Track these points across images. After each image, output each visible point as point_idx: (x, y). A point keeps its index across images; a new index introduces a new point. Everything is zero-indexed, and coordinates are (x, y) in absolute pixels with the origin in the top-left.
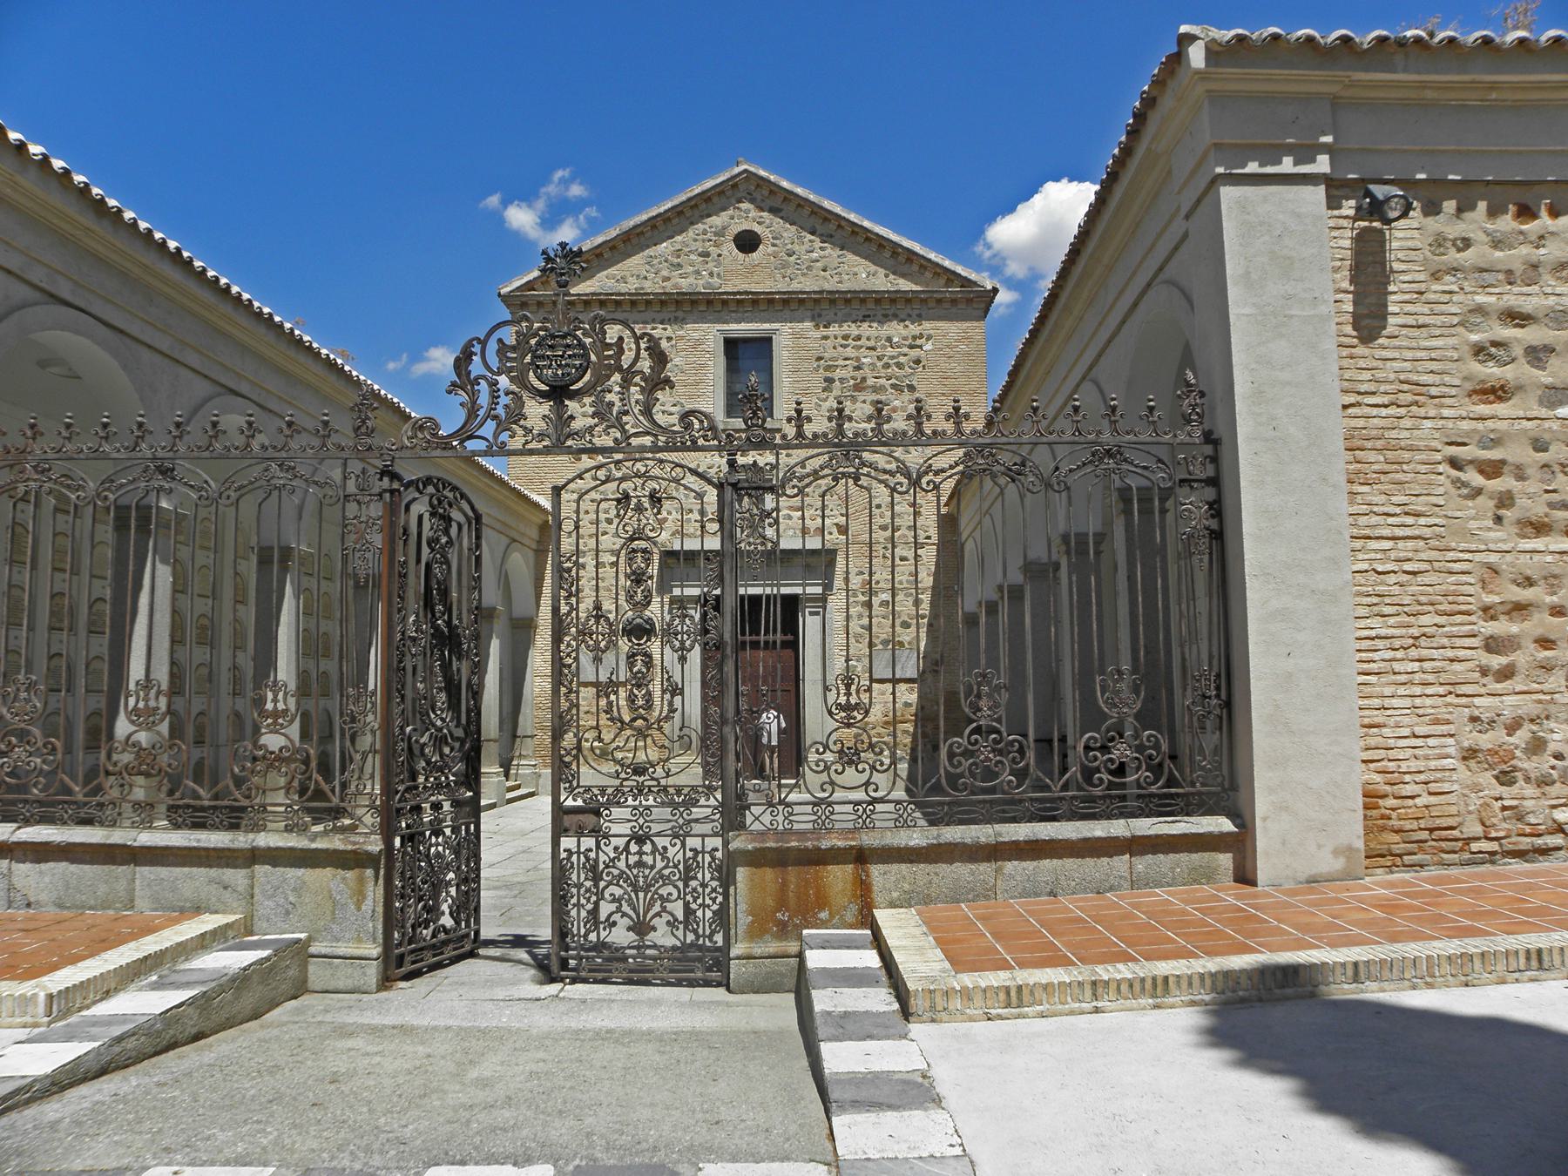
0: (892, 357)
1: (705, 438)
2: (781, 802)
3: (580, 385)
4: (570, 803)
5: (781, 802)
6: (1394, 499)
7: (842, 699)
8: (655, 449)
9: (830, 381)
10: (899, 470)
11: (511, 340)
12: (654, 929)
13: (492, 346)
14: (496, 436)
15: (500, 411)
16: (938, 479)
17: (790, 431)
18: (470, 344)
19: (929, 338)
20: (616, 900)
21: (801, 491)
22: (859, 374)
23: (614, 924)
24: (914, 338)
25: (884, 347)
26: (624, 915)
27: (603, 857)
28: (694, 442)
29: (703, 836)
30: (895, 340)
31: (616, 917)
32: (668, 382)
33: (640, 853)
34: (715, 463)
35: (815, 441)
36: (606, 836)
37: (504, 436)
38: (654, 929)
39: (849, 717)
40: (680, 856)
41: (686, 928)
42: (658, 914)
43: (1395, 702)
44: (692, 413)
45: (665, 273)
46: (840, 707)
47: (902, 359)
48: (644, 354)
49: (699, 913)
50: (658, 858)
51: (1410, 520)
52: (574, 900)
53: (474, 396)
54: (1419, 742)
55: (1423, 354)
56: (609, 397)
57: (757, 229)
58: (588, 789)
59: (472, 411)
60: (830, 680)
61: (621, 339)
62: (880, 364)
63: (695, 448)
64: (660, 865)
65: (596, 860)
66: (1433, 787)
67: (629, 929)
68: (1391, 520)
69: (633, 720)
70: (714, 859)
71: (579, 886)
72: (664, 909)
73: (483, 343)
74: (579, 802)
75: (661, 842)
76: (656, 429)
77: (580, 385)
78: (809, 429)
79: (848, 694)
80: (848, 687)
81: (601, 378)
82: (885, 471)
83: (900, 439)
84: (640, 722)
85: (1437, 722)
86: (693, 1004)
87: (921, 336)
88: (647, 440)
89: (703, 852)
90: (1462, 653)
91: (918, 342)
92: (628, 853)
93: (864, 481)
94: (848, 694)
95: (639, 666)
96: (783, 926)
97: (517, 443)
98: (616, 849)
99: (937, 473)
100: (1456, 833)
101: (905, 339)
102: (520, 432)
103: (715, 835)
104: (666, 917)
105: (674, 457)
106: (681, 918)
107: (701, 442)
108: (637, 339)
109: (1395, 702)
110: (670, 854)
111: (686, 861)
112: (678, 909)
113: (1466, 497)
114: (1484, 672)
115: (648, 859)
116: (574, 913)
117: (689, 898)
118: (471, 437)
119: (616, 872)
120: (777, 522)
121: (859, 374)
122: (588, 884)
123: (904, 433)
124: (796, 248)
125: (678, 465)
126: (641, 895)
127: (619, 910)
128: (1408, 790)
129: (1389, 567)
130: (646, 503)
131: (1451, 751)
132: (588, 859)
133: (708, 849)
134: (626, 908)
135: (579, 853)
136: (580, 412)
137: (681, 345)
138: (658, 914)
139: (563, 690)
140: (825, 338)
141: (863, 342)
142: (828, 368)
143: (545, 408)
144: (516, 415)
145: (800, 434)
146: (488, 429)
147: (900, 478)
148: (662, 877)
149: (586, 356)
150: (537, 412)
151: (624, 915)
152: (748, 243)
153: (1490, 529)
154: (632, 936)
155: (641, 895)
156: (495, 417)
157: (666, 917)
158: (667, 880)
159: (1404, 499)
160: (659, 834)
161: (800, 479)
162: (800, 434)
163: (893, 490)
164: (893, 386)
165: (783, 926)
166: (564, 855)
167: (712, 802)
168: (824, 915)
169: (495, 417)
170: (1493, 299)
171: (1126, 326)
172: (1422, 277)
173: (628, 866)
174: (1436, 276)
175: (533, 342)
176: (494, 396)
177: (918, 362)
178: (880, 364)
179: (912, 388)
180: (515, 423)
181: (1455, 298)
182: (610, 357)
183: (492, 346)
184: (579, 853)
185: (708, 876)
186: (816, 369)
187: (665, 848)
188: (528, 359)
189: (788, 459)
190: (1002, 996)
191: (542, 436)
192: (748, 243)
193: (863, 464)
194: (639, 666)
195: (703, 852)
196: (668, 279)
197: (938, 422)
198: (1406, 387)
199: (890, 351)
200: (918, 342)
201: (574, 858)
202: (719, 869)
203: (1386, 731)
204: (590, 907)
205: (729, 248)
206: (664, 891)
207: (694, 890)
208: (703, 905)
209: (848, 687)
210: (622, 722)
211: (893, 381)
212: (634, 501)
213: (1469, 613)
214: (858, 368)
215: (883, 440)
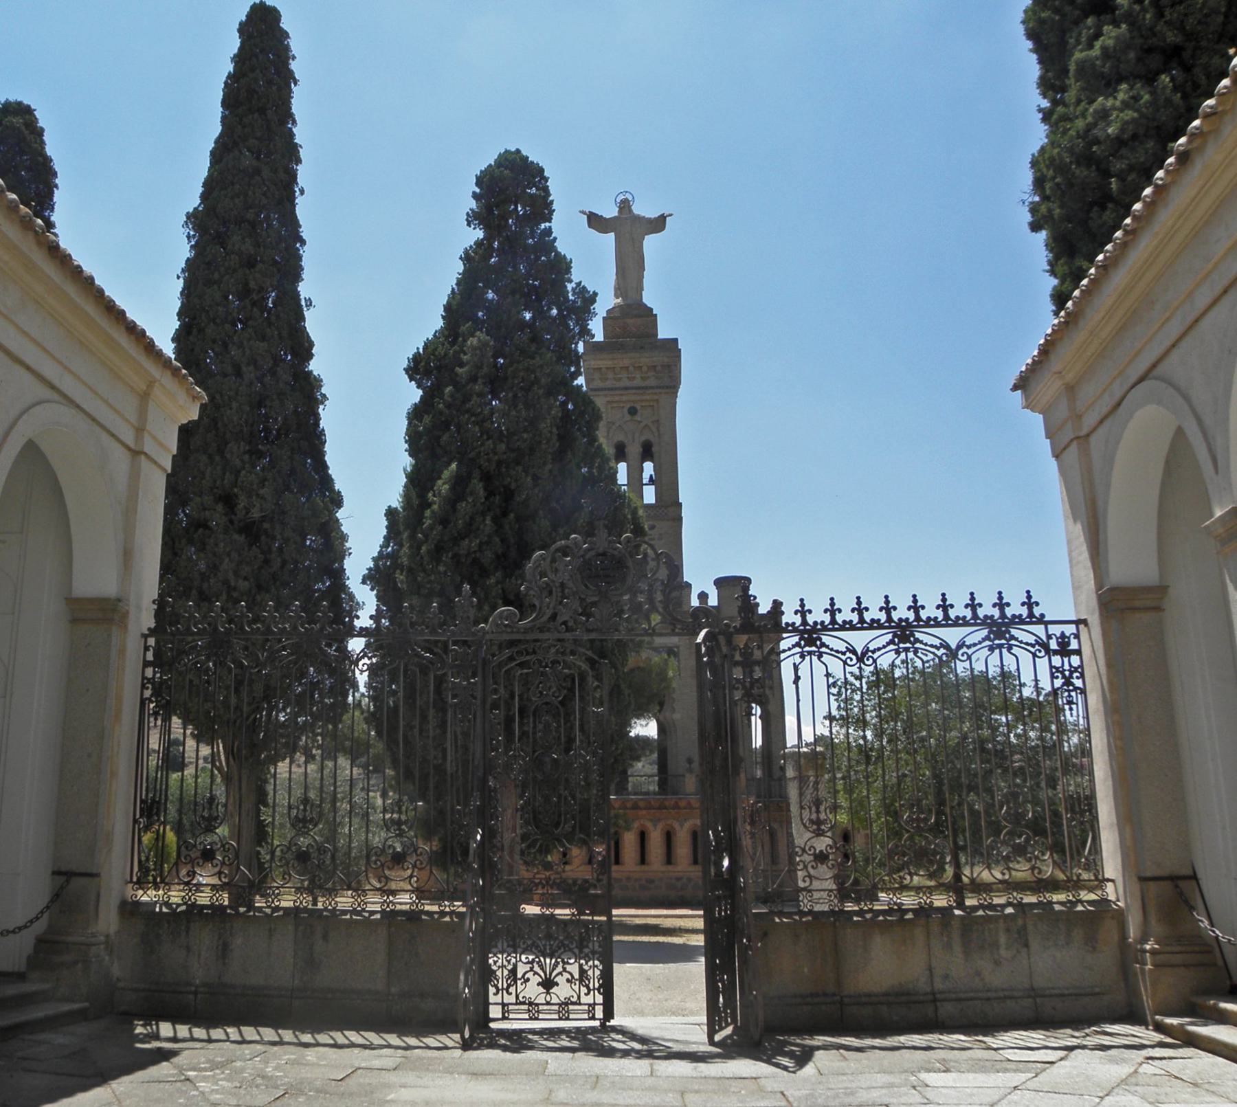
7: (814, 816)
10: (942, 646)
12: (557, 984)
16: (970, 652)
21: (969, 658)
23: (528, 980)
26: (536, 973)
31: (529, 975)
35: (875, 625)
38: (557, 984)
39: (819, 829)
42: (560, 973)
46: (812, 821)
49: (590, 973)
57: (643, 438)
67: (539, 984)
72: (565, 970)
79: (818, 812)
83: (848, 626)
86: (687, 1043)
93: (825, 658)
99: (969, 647)
106: (577, 976)
127: (532, 969)
134: (537, 968)
138: (560, 973)
147: (848, 654)
151: (536, 973)
157: (567, 976)
161: (874, 652)
163: (845, 663)
197: (959, 611)
204: (510, 967)
215: (835, 626)
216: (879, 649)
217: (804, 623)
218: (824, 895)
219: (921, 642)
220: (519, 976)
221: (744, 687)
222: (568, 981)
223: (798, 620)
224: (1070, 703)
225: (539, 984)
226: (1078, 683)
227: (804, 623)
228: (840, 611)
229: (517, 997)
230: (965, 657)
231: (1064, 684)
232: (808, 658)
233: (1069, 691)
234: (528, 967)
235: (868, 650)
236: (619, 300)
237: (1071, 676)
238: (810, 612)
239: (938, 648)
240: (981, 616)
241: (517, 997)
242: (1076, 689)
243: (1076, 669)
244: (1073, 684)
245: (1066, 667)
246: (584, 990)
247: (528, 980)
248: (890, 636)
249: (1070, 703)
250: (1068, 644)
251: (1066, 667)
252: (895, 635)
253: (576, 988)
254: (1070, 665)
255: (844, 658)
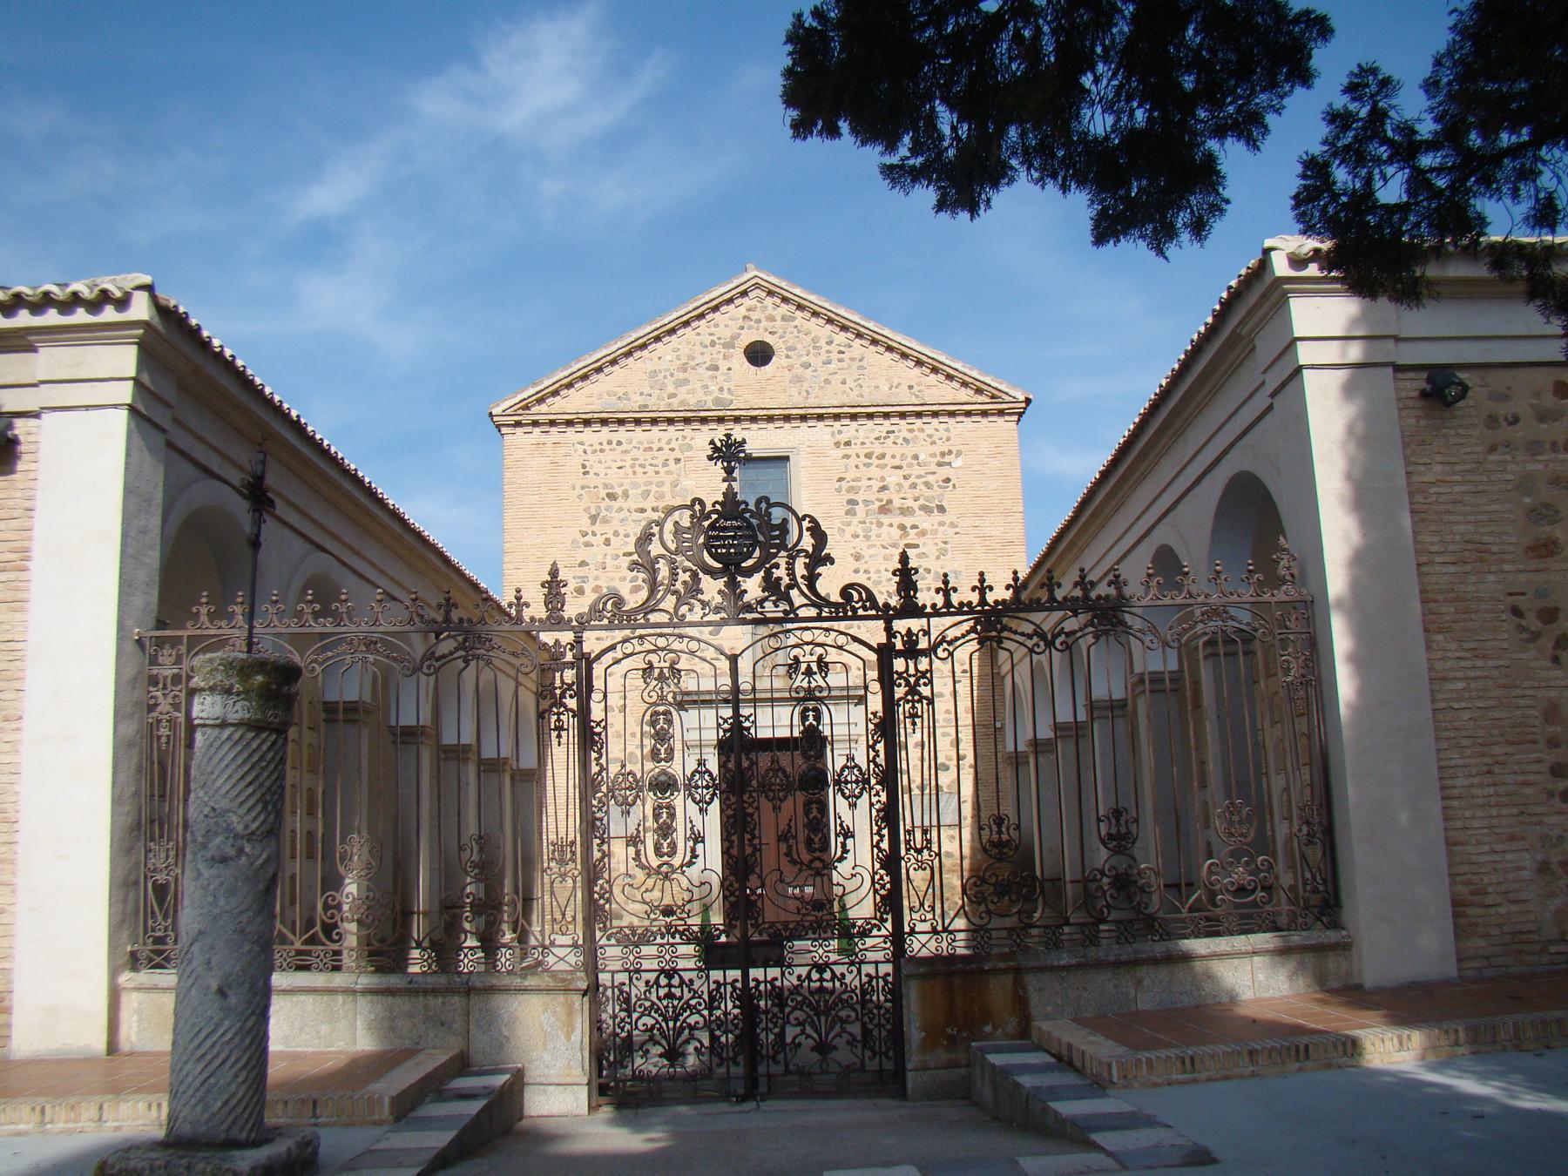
0: (919, 477)
1: (865, 609)
2: (945, 930)
3: (750, 562)
4: (756, 937)
5: (945, 930)
6: (1466, 645)
7: (1114, 830)
8: (819, 618)
9: (852, 502)
10: (1035, 633)
11: (686, 522)
12: (835, 1048)
13: (669, 526)
14: (676, 608)
15: (679, 586)
16: (1070, 640)
17: (939, 600)
18: (649, 526)
19: (959, 453)
20: (800, 1023)
22: (885, 496)
24: (943, 454)
25: (910, 465)
27: (634, 991)
28: (854, 610)
29: (876, 963)
30: (922, 457)
32: (829, 560)
33: (670, 985)
34: (874, 632)
36: (790, 966)
37: (684, 609)
38: (835, 1048)
39: (1119, 846)
40: (856, 982)
41: (864, 1047)
42: (839, 1035)
43: (1476, 824)
44: (851, 586)
45: (671, 389)
47: (930, 478)
48: (806, 534)
49: (876, 1033)
50: (837, 984)
51: (1479, 663)
52: (763, 1025)
53: (653, 572)
54: (1498, 858)
55: (1484, 517)
56: (777, 573)
57: (769, 339)
58: (772, 924)
59: (653, 586)
60: (984, 821)
61: (785, 521)
62: (906, 484)
63: (855, 617)
64: (687, 995)
65: (629, 995)
66: (1513, 896)
68: (1463, 664)
69: (811, 861)
70: (886, 982)
71: (766, 1012)
72: (844, 1030)
73: (660, 524)
74: (765, 937)
75: (687, 976)
76: (820, 602)
77: (750, 562)
78: (955, 599)
79: (1000, 832)
80: (999, 825)
81: (767, 557)
82: (1022, 634)
84: (817, 864)
85: (1512, 838)
87: (950, 452)
88: (813, 612)
89: (725, 984)
90: (1531, 778)
91: (947, 459)
92: (659, 986)
94: (1000, 832)
95: (815, 813)
96: (952, 1040)
97: (696, 615)
98: (647, 982)
100: (1535, 937)
101: (934, 455)
102: (698, 606)
103: (888, 961)
104: (846, 1037)
105: (835, 625)
107: (861, 612)
108: (800, 520)
109: (1476, 824)
110: (847, 980)
111: (710, 993)
112: (855, 1029)
113: (1528, 641)
114: (1551, 795)
115: (677, 992)
116: (763, 1036)
117: (866, 1019)
118: (653, 611)
119: (648, 1004)
120: (931, 682)
121: (885, 496)
122: (775, 1010)
123: (1039, 600)
124: (811, 359)
125: (842, 633)
126: (671, 1024)
127: (803, 1032)
128: (1490, 900)
129: (1463, 705)
130: (814, 667)
131: (1527, 863)
132: (621, 992)
133: (729, 980)
134: (809, 1030)
135: (613, 987)
136: (752, 587)
137: (690, 465)
138: (839, 1035)
139: (747, 836)
140: (847, 457)
141: (887, 460)
142: (850, 489)
143: (720, 584)
144: (694, 589)
145: (948, 604)
146: (669, 603)
147: (1035, 639)
148: (689, 1006)
149: (754, 537)
150: (712, 588)
151: (808, 1036)
152: (759, 354)
153: (1548, 669)
154: (816, 1056)
155: (823, 1018)
156: (675, 592)
157: (846, 1037)
158: (694, 1010)
159: (1473, 645)
160: (835, 963)
161: (950, 643)
162: (948, 604)
163: (1031, 651)
164: (923, 508)
165: (952, 1040)
166: (752, 984)
167: (884, 932)
168: (988, 1028)
169: (675, 592)
170: (1540, 467)
171: (1207, 479)
172: (1479, 449)
173: (659, 998)
174: (1492, 449)
175: (706, 524)
176: (674, 575)
177: (947, 480)
178: (906, 484)
179: (941, 509)
180: (693, 597)
181: (1509, 467)
182: (776, 537)
183: (669, 526)
184: (613, 987)
185: (730, 1005)
186: (839, 490)
187: (843, 975)
188: (701, 540)
189: (938, 625)
190: (1340, 1048)
191: (717, 610)
192: (759, 354)
193: (1005, 628)
194: (815, 813)
195: (877, 977)
196: (674, 395)
197: (927, 596)
198: (1470, 547)
199: (916, 470)
200: (947, 459)
201: (762, 987)
202: (891, 992)
203: (1469, 849)
204: (777, 1030)
205: (739, 360)
206: (843, 1014)
207: (871, 1011)
208: (879, 1025)
209: (999, 825)
210: (802, 863)
211: (921, 502)
212: (804, 666)
213: (1535, 742)
214: (884, 488)
216: (957, 639)
217: (983, 601)
218: (1004, 934)
219: (1010, 630)
220: (788, 1040)
221: (908, 683)
222: (848, 1042)
223: (974, 598)
224: (913, 716)
225: (813, 1049)
226: (925, 691)
227: (983, 601)
228: (991, 588)
229: (787, 1066)
230: (945, 654)
231: (907, 694)
232: (473, 664)
233: (913, 701)
234: (798, 1030)
235: (943, 640)
236: (844, 126)
237: (917, 683)
238: (955, 590)
239: (1030, 637)
240: (955, 603)
241: (787, 1066)
242: (922, 698)
243: (923, 675)
244: (919, 694)
245: (912, 671)
246: (868, 1054)
247: (799, 1045)
248: (971, 623)
249: (913, 716)
250: (917, 642)
251: (912, 671)
252: (977, 621)
253: (858, 1051)
254: (917, 670)
255: (1030, 643)
